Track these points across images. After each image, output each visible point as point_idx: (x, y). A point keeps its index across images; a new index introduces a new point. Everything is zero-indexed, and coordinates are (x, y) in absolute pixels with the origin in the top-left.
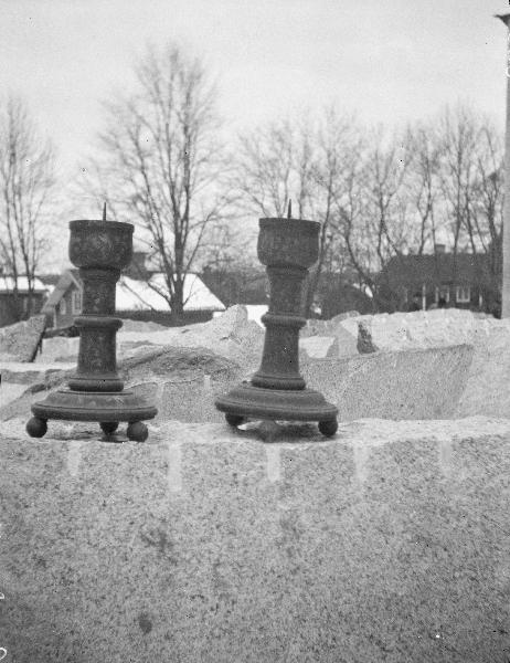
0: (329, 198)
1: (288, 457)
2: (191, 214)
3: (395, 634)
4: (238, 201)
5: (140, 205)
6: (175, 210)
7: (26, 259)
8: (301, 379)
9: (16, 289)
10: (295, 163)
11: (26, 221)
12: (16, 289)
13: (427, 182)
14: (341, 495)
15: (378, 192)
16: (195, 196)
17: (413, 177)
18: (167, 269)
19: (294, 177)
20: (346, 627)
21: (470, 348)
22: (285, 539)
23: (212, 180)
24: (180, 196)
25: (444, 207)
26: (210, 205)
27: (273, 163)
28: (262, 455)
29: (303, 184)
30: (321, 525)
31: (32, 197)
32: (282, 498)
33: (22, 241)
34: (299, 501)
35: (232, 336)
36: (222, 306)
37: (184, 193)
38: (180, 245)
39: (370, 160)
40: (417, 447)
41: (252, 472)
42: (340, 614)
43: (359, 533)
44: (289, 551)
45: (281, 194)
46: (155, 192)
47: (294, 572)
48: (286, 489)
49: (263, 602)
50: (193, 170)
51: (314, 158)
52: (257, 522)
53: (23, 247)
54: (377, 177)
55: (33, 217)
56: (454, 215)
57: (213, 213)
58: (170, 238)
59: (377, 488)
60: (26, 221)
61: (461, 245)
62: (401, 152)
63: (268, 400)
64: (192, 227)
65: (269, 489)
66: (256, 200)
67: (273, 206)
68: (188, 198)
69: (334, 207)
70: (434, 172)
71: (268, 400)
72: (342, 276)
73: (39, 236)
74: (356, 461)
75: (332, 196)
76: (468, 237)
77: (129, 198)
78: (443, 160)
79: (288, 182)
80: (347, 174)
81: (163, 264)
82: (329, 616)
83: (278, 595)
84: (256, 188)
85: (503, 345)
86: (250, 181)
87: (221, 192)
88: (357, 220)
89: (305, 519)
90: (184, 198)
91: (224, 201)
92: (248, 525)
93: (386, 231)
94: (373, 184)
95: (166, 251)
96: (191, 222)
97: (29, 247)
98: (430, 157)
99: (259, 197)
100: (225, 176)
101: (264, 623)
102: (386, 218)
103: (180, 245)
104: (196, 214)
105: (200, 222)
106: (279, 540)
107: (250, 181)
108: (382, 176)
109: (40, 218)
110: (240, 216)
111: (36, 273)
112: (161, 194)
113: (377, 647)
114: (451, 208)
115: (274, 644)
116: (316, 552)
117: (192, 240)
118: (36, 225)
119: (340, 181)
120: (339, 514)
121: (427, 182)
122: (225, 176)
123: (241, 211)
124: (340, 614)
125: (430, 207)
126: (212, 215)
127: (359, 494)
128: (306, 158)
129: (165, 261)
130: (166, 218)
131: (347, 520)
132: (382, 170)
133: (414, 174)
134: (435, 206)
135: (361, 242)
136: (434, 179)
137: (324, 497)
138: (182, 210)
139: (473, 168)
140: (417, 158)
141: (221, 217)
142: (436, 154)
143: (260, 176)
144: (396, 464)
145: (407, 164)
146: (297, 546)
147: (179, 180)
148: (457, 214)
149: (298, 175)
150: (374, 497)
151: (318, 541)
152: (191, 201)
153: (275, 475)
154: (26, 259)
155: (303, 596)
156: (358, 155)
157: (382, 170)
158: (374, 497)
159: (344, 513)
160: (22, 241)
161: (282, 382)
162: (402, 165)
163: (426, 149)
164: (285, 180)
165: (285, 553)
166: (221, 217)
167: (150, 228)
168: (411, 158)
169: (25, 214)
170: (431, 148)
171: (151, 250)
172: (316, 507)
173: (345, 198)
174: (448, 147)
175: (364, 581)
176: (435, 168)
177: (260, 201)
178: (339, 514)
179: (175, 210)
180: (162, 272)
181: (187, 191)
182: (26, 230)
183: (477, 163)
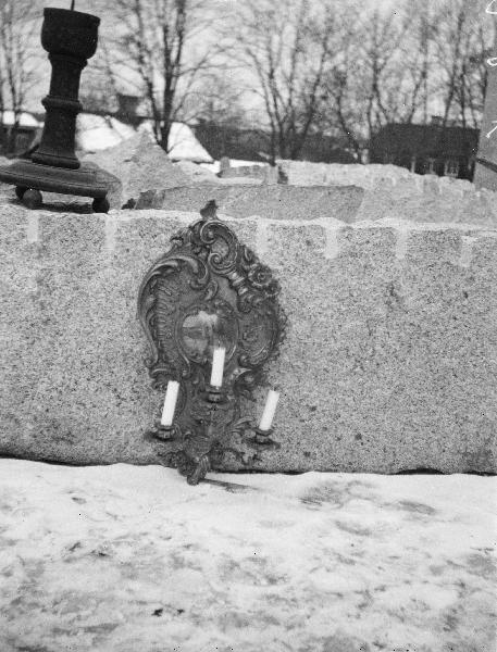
0: (323, 56)
1: (45, 222)
2: (183, 61)
3: (129, 383)
4: (231, 51)
5: (133, 46)
6: (167, 52)
7: (13, 90)
8: (76, 159)
9: (17, 123)
10: (293, 17)
11: (15, 51)
12: (17, 123)
13: (424, 48)
14: (93, 261)
15: (374, 55)
16: (188, 42)
17: (411, 41)
18: (156, 117)
19: (290, 30)
20: (86, 374)
21: (360, 190)
22: (39, 293)
23: (206, 27)
24: (173, 41)
25: (438, 75)
26: (201, 51)
27: (270, 14)
28: (23, 220)
29: (298, 39)
30: (72, 285)
31: (22, 27)
32: (39, 257)
33: (10, 72)
34: (55, 262)
35: (135, 159)
36: (209, 158)
37: (177, 39)
38: (169, 93)
39: (367, 20)
40: (159, 224)
41: (14, 233)
42: (83, 363)
43: (103, 295)
44: (42, 304)
45: (275, 48)
46: (148, 34)
47: (46, 323)
48: (43, 251)
49: (17, 345)
50: (188, 13)
51: (312, 13)
52: (16, 276)
53: (11, 78)
54: (374, 39)
55: (22, 49)
56: (448, 85)
57: (204, 61)
58: (159, 84)
59: (123, 258)
60: (15, 51)
61: (451, 117)
62: (401, 15)
63: (37, 172)
64: (183, 73)
65: (29, 249)
66: (249, 52)
67: (266, 59)
68: (181, 43)
69: (328, 66)
70: (433, 39)
71: (37, 172)
72: (332, 140)
73: (27, 68)
74: (107, 232)
75: (328, 53)
76: (460, 108)
77: (122, 37)
78: (443, 26)
79: (284, 36)
80: (344, 33)
81: (150, 109)
82: (73, 362)
83: (30, 341)
84: (252, 39)
85: (408, 196)
86: (245, 31)
87: (214, 40)
88: (351, 80)
89: (58, 278)
90: (176, 43)
91: (215, 50)
92: (8, 278)
93: (378, 95)
94: (369, 45)
95: (155, 95)
96: (182, 69)
97: (17, 77)
98: (430, 22)
99: (253, 48)
100: (221, 24)
101: (16, 362)
102: (380, 82)
103: (169, 93)
104: (187, 60)
105: (190, 70)
106: (35, 294)
107: (245, 31)
108: (379, 38)
109: (29, 50)
110: (231, 67)
111: (24, 107)
112: (152, 38)
113: (113, 395)
114: (446, 78)
115: (24, 382)
116: (67, 308)
117: (181, 85)
118: (25, 56)
119: (334, 40)
120: (89, 278)
121: (424, 48)
122: (221, 24)
123: (233, 62)
124: (83, 363)
125: (424, 75)
126: (202, 64)
127: (107, 262)
128: (303, 13)
129: (153, 106)
130: (157, 63)
131: (95, 284)
132: (380, 31)
133: (412, 39)
134: (429, 73)
135: (352, 104)
136: (432, 45)
137: (77, 262)
138: (174, 55)
139: (473, 38)
140: (417, 22)
141: (211, 66)
142: (437, 20)
143: (256, 26)
144: (140, 238)
145: (406, 27)
146: (49, 300)
147: (172, 23)
148: (451, 85)
149: (294, 30)
150: (119, 264)
151: (68, 298)
152: (184, 47)
153: (34, 237)
154: (13, 90)
155: (51, 343)
156: (357, 14)
157: (380, 31)
158: (119, 264)
159: (94, 277)
160: (10, 72)
161: (65, 160)
162: (400, 28)
163: (426, 14)
164: (280, 33)
165: (38, 306)
166: (211, 66)
167: (140, 71)
168: (410, 21)
169: (15, 45)
170: (432, 13)
171: (140, 94)
172: (69, 269)
173: (340, 57)
174: (449, 13)
175: (105, 336)
176: (434, 34)
177: (254, 53)
178: (89, 278)
179: (167, 52)
180: (150, 118)
181: (181, 37)
182: (15, 60)
183: (477, 33)
